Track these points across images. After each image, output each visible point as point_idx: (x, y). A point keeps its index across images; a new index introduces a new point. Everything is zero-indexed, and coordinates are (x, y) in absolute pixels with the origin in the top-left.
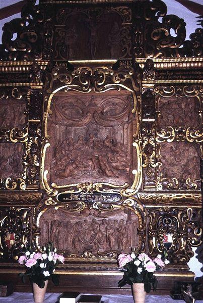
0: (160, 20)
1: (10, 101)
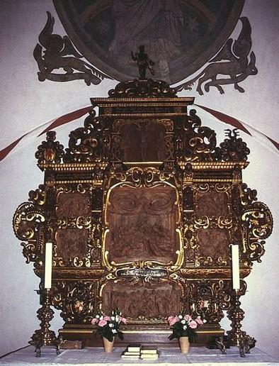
0: (196, 130)
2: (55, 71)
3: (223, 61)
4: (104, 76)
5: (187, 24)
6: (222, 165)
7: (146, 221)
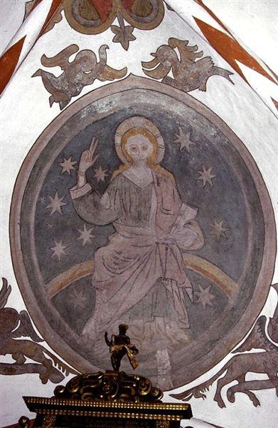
3: (253, 351)
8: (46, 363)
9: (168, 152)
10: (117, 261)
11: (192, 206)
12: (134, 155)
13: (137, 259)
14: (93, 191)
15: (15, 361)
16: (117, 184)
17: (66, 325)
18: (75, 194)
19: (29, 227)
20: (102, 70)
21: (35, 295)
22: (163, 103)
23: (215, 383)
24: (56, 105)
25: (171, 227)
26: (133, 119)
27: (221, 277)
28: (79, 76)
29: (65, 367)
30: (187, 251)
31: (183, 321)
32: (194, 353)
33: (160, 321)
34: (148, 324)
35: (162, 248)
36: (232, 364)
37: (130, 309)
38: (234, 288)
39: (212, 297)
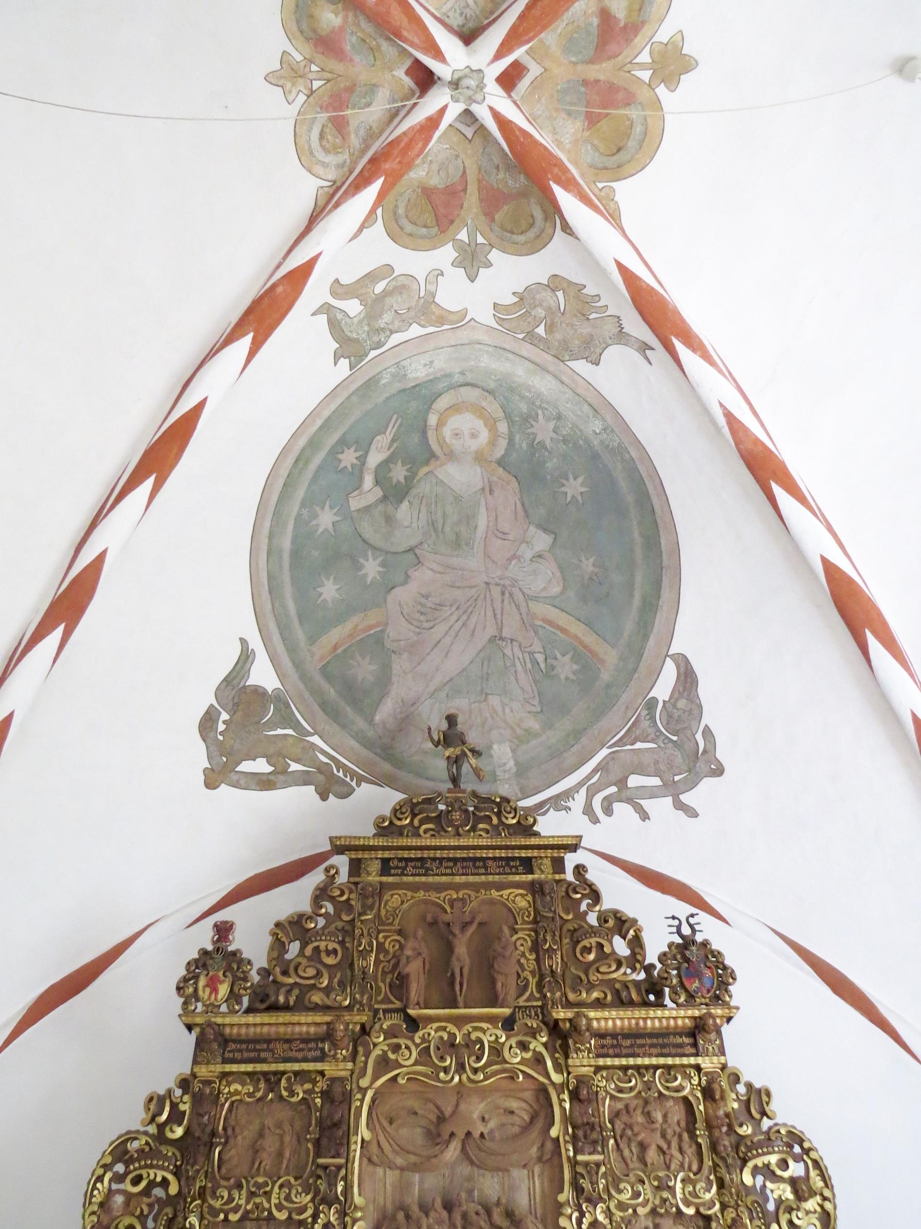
0: (592, 919)
1: (277, 1106)
2: (246, 766)
3: (639, 745)
4: (360, 780)
5: (553, 668)
6: (673, 1014)
7: (470, 1192)
8: (322, 769)
9: (514, 445)
10: (423, 610)
11: (545, 530)
12: (456, 444)
13: (454, 608)
14: (385, 498)
15: (273, 768)
16: (424, 488)
17: (348, 709)
18: (355, 503)
19: (281, 558)
20: (426, 309)
21: (293, 662)
22: (520, 372)
23: (583, 790)
24: (344, 363)
25: (510, 560)
26: (462, 389)
27: (589, 638)
28: (387, 317)
29: (353, 774)
30: (536, 599)
31: (531, 701)
32: (550, 748)
33: (494, 701)
34: (476, 704)
35: (496, 592)
36: (608, 763)
37: (447, 683)
38: (611, 656)
39: (575, 667)
